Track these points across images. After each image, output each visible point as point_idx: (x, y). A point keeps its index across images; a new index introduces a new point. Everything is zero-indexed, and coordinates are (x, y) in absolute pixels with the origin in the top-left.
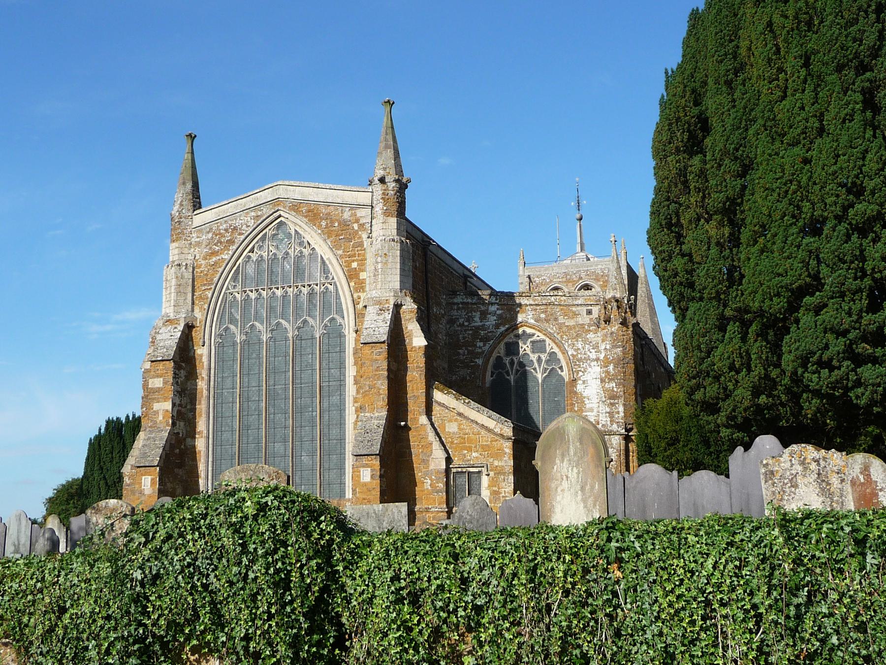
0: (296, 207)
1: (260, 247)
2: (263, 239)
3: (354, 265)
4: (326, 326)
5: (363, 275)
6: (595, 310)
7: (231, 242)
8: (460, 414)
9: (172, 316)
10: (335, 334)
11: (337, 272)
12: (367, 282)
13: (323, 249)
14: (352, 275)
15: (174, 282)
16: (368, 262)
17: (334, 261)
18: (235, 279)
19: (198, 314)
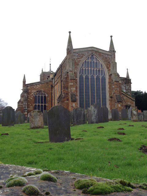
0: (96, 52)
1: (88, 59)
2: (89, 58)
3: (108, 66)
4: (91, 76)
5: (110, 68)
6: (125, 81)
7: (82, 57)
8: (126, 96)
9: (71, 70)
10: (104, 79)
11: (105, 67)
12: (111, 69)
13: (101, 62)
14: (108, 68)
15: (71, 63)
16: (111, 66)
17: (104, 65)
18: (83, 65)
19: (76, 71)
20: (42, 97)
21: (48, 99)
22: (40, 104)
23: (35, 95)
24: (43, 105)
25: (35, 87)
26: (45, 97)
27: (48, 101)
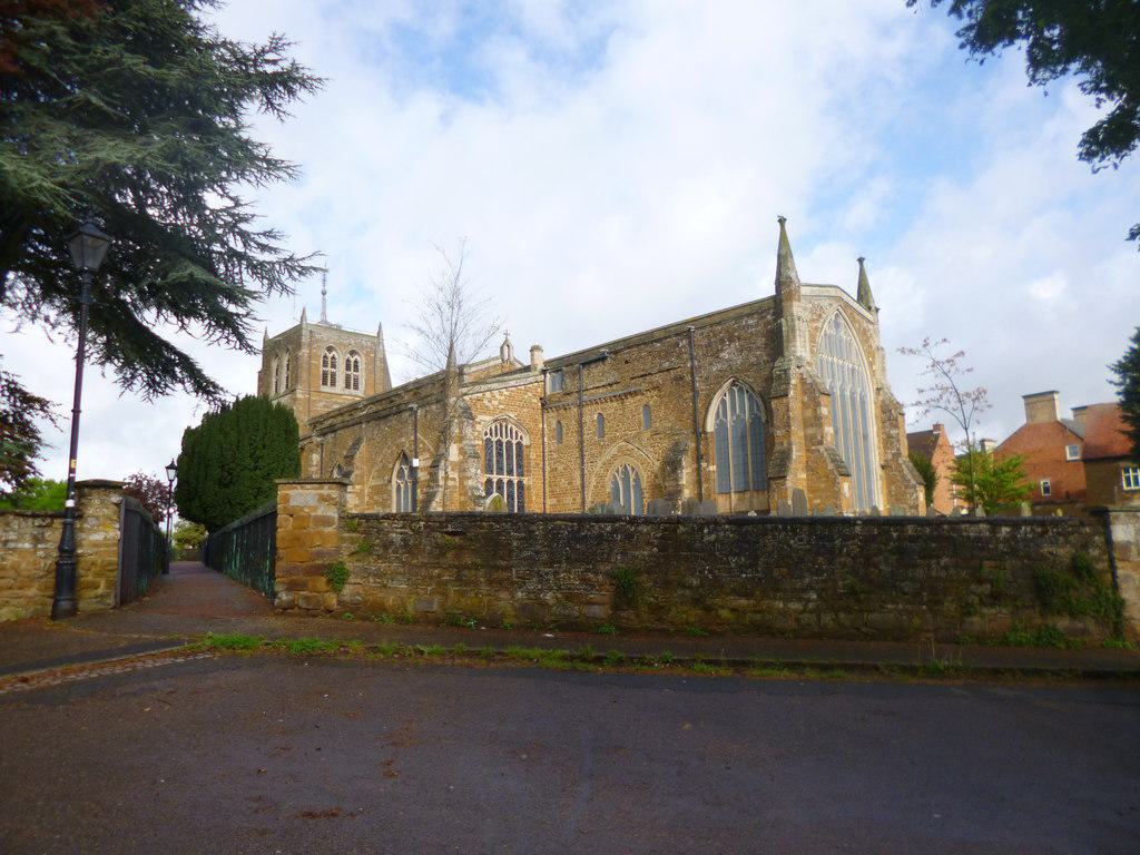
20: (509, 444)
21: (533, 456)
22: (505, 478)
23: (486, 434)
24: (515, 479)
25: (486, 402)
26: (519, 445)
27: (533, 464)
